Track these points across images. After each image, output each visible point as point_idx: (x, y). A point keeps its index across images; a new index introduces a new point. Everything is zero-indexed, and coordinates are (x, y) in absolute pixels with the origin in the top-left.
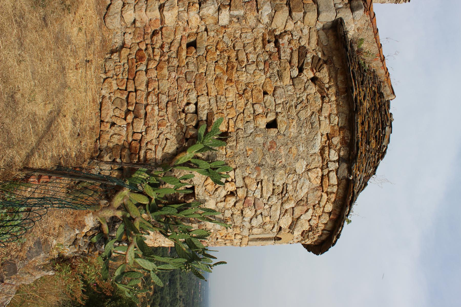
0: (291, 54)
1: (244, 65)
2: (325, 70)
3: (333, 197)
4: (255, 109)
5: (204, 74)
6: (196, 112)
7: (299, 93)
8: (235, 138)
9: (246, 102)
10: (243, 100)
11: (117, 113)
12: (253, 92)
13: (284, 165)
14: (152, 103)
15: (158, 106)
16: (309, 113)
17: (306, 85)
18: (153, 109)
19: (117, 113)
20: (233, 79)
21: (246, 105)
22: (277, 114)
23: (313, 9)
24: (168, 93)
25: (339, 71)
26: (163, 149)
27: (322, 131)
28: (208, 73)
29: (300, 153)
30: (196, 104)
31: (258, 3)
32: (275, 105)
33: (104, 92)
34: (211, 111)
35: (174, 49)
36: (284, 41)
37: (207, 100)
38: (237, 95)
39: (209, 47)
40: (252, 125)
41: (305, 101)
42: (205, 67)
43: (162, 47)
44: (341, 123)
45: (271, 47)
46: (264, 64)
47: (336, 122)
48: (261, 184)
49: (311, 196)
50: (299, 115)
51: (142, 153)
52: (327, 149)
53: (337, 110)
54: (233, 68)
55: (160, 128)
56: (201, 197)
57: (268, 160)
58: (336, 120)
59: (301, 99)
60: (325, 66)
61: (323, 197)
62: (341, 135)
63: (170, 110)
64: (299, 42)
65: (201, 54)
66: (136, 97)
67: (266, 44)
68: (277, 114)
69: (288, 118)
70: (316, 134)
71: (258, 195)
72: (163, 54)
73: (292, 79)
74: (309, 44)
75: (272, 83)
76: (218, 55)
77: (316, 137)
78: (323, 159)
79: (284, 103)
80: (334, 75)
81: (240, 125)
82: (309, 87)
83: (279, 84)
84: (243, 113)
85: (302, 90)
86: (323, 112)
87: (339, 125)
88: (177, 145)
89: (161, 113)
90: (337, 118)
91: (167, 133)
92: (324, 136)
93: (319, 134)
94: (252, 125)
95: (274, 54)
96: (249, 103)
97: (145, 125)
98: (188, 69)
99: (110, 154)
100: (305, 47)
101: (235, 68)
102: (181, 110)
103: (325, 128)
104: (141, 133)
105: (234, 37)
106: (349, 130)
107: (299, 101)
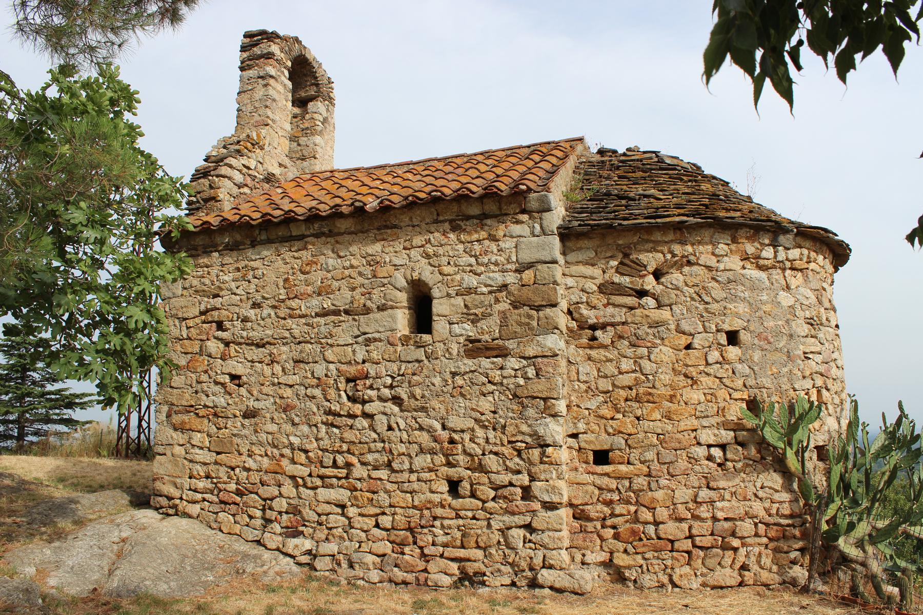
0: (614, 305)
1: (643, 378)
2: (644, 257)
3: (813, 254)
4: (714, 361)
5: (662, 436)
6: (723, 447)
7: (683, 298)
8: (756, 391)
9: (703, 375)
10: (702, 379)
11: (728, 561)
12: (690, 363)
13: (786, 322)
14: (711, 511)
15: (715, 502)
16: (715, 285)
17: (670, 286)
18: (722, 510)
19: (728, 561)
20: (669, 393)
22: (718, 331)
23: (547, 269)
24: (695, 488)
25: (646, 237)
26: (777, 491)
27: (739, 268)
28: (660, 431)
29: (770, 300)
30: (709, 446)
31: (541, 354)
32: (706, 332)
33: (695, 586)
34: (721, 424)
35: (613, 484)
36: (591, 316)
37: (704, 431)
38: (695, 387)
39: (611, 430)
40: (739, 367)
41: (697, 289)
42: (650, 435)
43: (609, 503)
44: (728, 240)
46: (639, 347)
47: (726, 247)
48: (807, 353)
49: (815, 284)
50: (719, 299)
51: (785, 522)
52: (761, 262)
53: (707, 244)
54: (650, 394)
55: (748, 497)
56: (826, 437)
57: (781, 345)
58: (722, 248)
59: (694, 295)
60: (633, 256)
61: (813, 268)
62: (744, 241)
63: (722, 484)
64: (592, 293)
65: (623, 442)
66: (703, 536)
67: (601, 344)
68: (718, 331)
69: (725, 314)
70: (743, 276)
71: (819, 358)
72: (623, 500)
73: (660, 306)
74: (593, 278)
75: (672, 336)
76: (624, 416)
77: (748, 277)
78: (774, 267)
79: (702, 319)
80: (651, 245)
82: (674, 282)
83: (673, 327)
84: (720, 378)
85: (679, 293)
86: (712, 265)
87: (729, 242)
88: (771, 471)
89: (727, 496)
90: (721, 246)
91: (755, 487)
92: (745, 266)
94: (739, 367)
95: (619, 332)
96: (706, 370)
97: (743, 520)
98: (653, 461)
99: (786, 567)
100: (601, 284)
101: (650, 390)
102: (719, 469)
103: (733, 262)
104: (756, 525)
105: (586, 391)
106: (737, 229)
107: (697, 298)
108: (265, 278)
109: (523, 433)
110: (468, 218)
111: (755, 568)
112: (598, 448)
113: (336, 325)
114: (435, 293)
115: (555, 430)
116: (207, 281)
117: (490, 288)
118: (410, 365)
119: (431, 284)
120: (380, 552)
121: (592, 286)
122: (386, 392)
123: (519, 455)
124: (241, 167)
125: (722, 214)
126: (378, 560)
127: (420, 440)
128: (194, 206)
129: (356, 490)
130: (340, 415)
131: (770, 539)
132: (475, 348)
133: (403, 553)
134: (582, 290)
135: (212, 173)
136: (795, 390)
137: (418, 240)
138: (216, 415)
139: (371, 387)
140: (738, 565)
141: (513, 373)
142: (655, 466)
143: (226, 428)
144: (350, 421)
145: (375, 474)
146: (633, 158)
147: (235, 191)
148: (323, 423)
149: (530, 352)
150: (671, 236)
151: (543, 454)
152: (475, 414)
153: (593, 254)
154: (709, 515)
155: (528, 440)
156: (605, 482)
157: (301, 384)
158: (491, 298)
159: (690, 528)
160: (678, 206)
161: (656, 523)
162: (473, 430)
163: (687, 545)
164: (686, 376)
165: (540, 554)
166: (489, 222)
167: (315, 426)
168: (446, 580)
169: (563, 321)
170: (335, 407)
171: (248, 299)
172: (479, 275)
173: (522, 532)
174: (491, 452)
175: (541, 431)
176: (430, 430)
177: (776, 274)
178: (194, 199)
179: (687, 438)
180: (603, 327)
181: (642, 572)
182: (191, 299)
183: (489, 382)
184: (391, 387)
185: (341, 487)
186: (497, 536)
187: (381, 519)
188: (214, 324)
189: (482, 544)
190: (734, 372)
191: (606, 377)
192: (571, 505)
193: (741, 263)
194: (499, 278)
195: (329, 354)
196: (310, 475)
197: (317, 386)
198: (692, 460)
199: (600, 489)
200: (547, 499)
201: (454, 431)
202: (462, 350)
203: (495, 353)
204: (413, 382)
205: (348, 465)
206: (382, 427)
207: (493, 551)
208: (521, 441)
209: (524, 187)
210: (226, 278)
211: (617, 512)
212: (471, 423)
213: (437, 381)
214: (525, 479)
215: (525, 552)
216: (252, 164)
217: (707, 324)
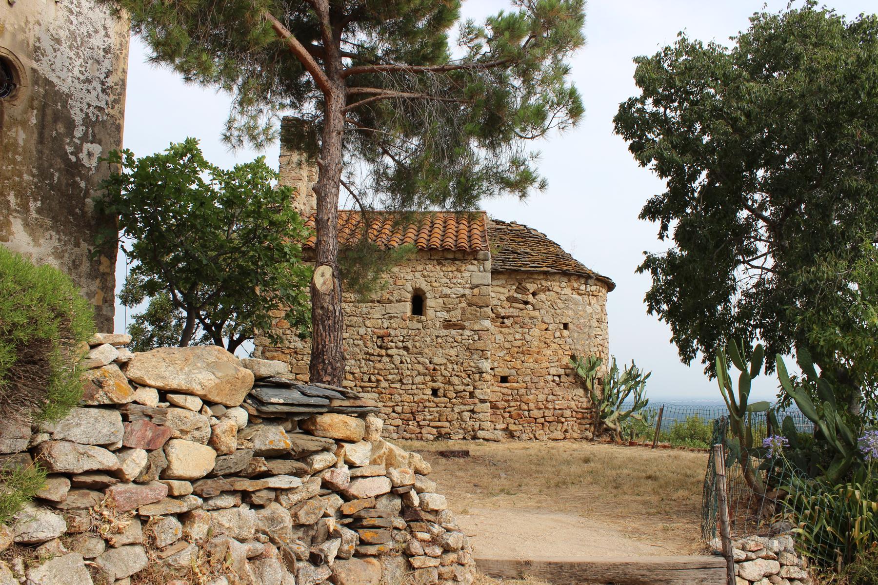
0: (514, 308)
2: (528, 286)
6: (559, 376)
16: (559, 301)
18: (558, 405)
19: (559, 428)
30: (554, 376)
35: (510, 392)
36: (503, 312)
43: (507, 401)
52: (580, 292)
58: (564, 284)
71: (601, 338)
73: (534, 309)
74: (504, 294)
78: (585, 294)
81: (568, 347)
83: (540, 320)
89: (561, 399)
103: (568, 291)
110: (446, 259)
111: (570, 431)
112: (503, 375)
113: (372, 308)
114: (428, 295)
115: (486, 365)
118: (413, 331)
120: (396, 424)
121: (503, 298)
122: (400, 344)
123: (469, 377)
126: (395, 428)
127: (418, 369)
129: (382, 393)
130: (373, 355)
131: (577, 419)
132: (448, 324)
133: (408, 425)
137: (420, 268)
138: (296, 353)
139: (392, 341)
140: (563, 430)
142: (529, 384)
143: (302, 360)
144: (379, 359)
145: (393, 385)
148: (363, 359)
149: (476, 328)
150: (541, 277)
151: (481, 376)
152: (447, 357)
153: (504, 282)
154: (552, 407)
155: (474, 370)
156: (506, 391)
157: (351, 338)
158: (458, 300)
159: (544, 413)
161: (529, 410)
162: (446, 364)
163: (542, 420)
164: (545, 343)
165: (478, 423)
166: (457, 262)
167: (359, 360)
168: (432, 437)
170: (371, 351)
173: (469, 413)
174: (455, 375)
175: (480, 366)
176: (423, 364)
179: (544, 371)
180: (508, 317)
181: (93, 507)
184: (403, 341)
185: (374, 392)
186: (456, 416)
187: (396, 408)
189: (449, 419)
191: (508, 341)
192: (490, 402)
194: (461, 291)
195: (368, 323)
196: (355, 386)
197: (361, 339)
198: (546, 381)
199: (503, 394)
200: (482, 398)
202: (442, 325)
203: (458, 327)
204: (415, 340)
205: (378, 381)
206: (397, 362)
207: (455, 423)
211: (511, 405)
212: (445, 361)
213: (428, 339)
214: (471, 388)
215: (470, 423)
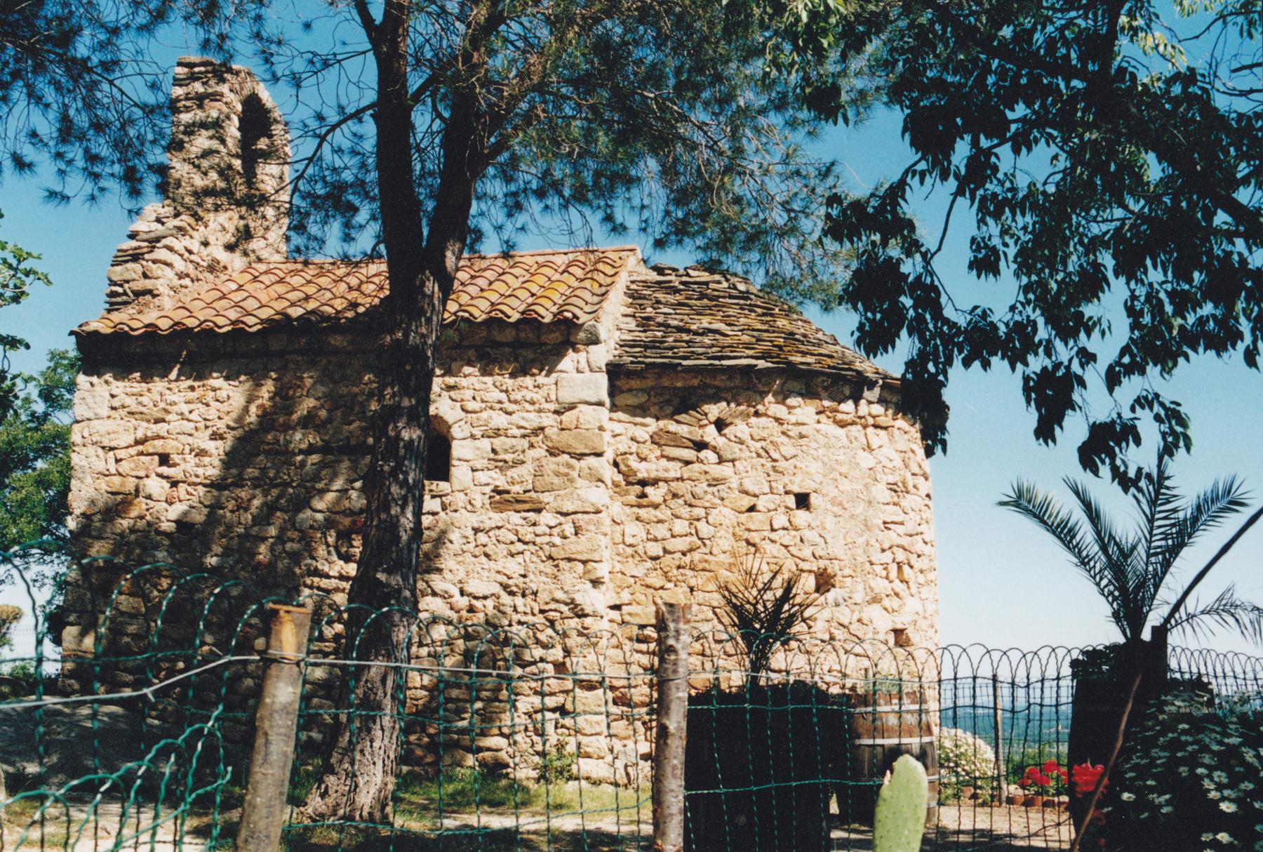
1: (699, 542)
8: (827, 562)
12: (753, 528)
16: (784, 439)
21: (773, 541)
22: (787, 493)
36: (643, 470)
41: (763, 444)
42: (705, 608)
45: (655, 494)
49: (902, 445)
52: (839, 416)
54: (706, 561)
64: (644, 443)
71: (900, 529)
73: (721, 461)
78: (853, 423)
82: (739, 435)
84: (786, 547)
93: (818, 426)
100: (655, 433)
107: (763, 453)
108: (231, 401)
109: (557, 601)
114: (456, 431)
116: (145, 400)
117: (523, 431)
119: (451, 421)
124: (183, 251)
125: (797, 359)
128: (119, 299)
132: (501, 499)
134: (632, 439)
135: (147, 256)
136: (872, 564)
141: (548, 531)
146: (698, 279)
147: (176, 282)
160: (748, 346)
164: (748, 543)
169: (609, 474)
171: (207, 427)
172: (510, 414)
177: (855, 430)
178: (120, 290)
180: (655, 482)
182: (122, 422)
183: (519, 540)
188: (156, 458)
190: (802, 540)
191: (656, 540)
193: (817, 417)
194: (533, 420)
201: (476, 598)
203: (527, 506)
207: (518, 738)
208: (555, 610)
209: (569, 315)
210: (174, 398)
214: (557, 654)
216: (195, 245)
217: (774, 484)
